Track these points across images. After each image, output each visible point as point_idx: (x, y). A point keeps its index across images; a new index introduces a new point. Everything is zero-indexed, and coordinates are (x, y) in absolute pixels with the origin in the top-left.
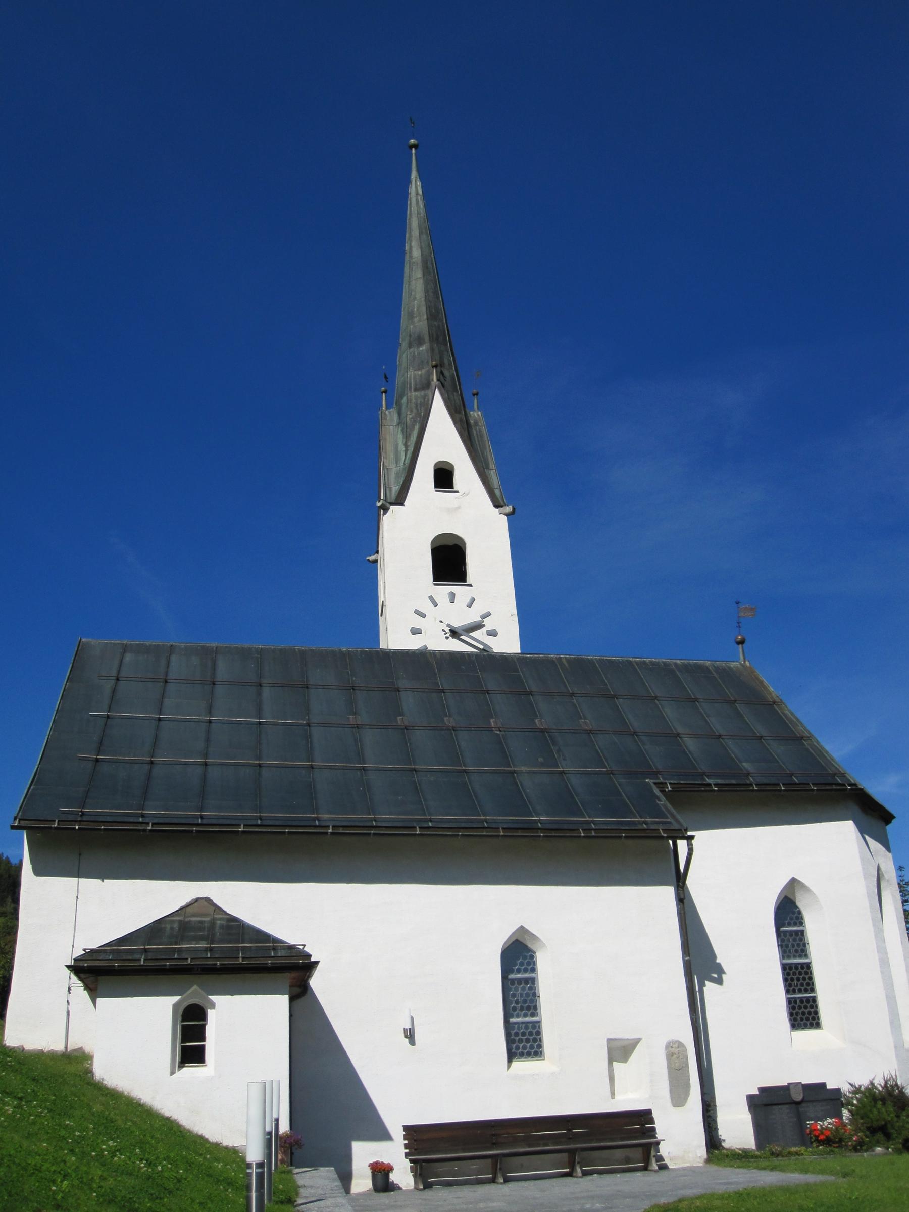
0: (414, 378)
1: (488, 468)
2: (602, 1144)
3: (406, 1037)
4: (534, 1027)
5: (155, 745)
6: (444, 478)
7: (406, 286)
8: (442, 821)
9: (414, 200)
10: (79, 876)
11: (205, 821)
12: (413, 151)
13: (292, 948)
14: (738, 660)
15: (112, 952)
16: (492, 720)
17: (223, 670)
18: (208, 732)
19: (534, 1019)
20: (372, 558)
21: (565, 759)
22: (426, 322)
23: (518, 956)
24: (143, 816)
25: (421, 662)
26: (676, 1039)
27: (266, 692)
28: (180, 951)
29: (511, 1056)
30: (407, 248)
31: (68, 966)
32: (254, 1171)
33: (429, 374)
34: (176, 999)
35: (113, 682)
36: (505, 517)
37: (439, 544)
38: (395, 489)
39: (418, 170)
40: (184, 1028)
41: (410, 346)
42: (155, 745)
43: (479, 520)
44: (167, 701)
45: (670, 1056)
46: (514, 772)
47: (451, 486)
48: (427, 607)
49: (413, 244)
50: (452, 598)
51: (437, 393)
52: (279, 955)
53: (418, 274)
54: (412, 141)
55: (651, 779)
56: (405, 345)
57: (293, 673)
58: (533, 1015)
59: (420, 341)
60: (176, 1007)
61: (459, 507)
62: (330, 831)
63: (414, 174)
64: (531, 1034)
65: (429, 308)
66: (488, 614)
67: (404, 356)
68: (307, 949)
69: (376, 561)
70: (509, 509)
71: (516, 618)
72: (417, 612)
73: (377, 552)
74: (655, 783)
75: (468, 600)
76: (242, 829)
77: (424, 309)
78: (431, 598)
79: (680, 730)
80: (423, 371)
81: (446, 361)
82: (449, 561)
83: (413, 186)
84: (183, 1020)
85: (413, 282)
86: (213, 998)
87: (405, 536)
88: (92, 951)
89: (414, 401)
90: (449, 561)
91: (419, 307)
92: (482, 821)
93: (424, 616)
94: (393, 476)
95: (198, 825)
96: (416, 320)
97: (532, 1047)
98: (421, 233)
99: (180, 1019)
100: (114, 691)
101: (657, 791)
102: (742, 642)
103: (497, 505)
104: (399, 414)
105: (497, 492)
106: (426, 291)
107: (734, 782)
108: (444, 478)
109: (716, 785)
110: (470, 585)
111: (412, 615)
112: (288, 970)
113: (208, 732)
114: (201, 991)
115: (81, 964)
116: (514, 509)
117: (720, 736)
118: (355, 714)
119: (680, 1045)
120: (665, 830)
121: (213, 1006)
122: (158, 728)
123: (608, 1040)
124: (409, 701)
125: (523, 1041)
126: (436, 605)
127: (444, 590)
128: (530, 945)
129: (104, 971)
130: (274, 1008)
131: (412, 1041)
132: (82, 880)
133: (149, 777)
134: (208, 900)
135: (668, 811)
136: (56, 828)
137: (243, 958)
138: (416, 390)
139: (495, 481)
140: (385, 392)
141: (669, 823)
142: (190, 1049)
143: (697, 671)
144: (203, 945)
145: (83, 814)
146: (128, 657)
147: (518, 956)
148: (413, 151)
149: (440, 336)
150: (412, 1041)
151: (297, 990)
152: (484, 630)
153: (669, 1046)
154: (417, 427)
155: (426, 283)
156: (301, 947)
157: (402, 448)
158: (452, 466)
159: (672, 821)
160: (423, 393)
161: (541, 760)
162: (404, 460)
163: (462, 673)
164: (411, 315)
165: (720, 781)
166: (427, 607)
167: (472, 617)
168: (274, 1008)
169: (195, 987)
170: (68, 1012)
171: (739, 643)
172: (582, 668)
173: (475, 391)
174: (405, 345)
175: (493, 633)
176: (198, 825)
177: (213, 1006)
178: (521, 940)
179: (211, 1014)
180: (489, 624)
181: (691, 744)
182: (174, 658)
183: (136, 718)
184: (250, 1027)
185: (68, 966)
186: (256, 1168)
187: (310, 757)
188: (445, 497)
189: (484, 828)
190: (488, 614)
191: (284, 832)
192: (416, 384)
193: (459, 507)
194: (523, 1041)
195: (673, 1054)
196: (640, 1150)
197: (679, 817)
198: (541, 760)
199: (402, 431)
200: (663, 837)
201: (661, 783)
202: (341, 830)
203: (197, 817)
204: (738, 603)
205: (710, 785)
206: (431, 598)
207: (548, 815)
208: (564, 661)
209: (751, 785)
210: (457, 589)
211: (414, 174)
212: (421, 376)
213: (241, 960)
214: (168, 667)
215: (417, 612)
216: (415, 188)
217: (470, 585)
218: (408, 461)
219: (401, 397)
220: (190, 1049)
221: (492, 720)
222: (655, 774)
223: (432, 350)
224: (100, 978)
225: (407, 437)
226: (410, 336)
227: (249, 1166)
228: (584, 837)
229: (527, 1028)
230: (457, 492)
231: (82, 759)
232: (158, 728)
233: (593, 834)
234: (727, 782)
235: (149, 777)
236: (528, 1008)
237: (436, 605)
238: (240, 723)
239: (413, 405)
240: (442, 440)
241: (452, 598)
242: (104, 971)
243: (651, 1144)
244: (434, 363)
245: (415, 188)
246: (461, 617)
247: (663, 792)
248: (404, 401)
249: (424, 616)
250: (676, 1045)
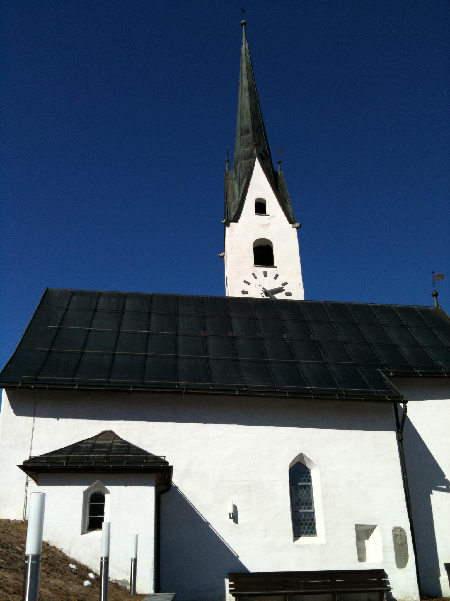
0: (244, 152)
1: (286, 202)
2: (353, 589)
3: (230, 518)
4: (310, 516)
5: (85, 344)
6: (261, 207)
7: (239, 102)
8: (252, 387)
9: (244, 54)
10: (34, 416)
11: (110, 385)
12: (244, 26)
13: (157, 458)
14: (432, 304)
15: (48, 458)
16: (284, 335)
17: (129, 305)
18: (117, 338)
19: (310, 511)
20: (221, 255)
21: (328, 357)
22: (250, 121)
23: (299, 474)
24: (73, 381)
25: (244, 304)
26: (399, 526)
27: (153, 318)
28: (88, 458)
29: (297, 535)
30: (240, 81)
31: (19, 466)
32: (30, 562)
33: (253, 150)
34: (86, 487)
35: (63, 311)
36: (295, 230)
37: (257, 245)
38: (233, 214)
39: (246, 38)
40: (91, 506)
41: (242, 134)
42: (85, 344)
43: (282, 233)
44: (95, 322)
45: (395, 536)
46: (298, 363)
47: (265, 213)
48: (251, 279)
49: (243, 78)
50: (265, 274)
51: (257, 161)
52: (149, 462)
53: (246, 94)
54: (243, 21)
55: (380, 369)
56: (239, 134)
57: (169, 306)
58: (309, 508)
59: (247, 132)
60: (86, 493)
61: (269, 224)
62: (185, 391)
63: (244, 39)
64: (308, 520)
65: (252, 113)
66: (286, 284)
67: (238, 141)
68: (167, 459)
69: (223, 256)
70: (297, 225)
71: (302, 286)
72: (245, 282)
73: (224, 251)
74: (383, 371)
75: (274, 275)
76: (132, 389)
77: (249, 114)
78: (253, 274)
79: (398, 342)
80: (249, 149)
81: (262, 143)
82: (263, 254)
83: (243, 46)
84: (91, 502)
85: (243, 100)
86: (108, 487)
87: (239, 239)
88: (36, 458)
89: (243, 165)
90: (263, 254)
91: (246, 113)
92: (276, 388)
93: (249, 284)
94: (232, 206)
95: (105, 386)
96: (245, 120)
97: (309, 528)
98: (248, 72)
99: (88, 500)
100: (64, 315)
101: (384, 376)
102: (436, 295)
103: (291, 222)
104: (236, 173)
105: (291, 216)
106: (251, 104)
107: (432, 372)
108: (261, 207)
109: (420, 373)
110: (276, 267)
111: (241, 279)
112: (155, 471)
113: (117, 338)
114: (100, 483)
115: (27, 465)
116: (301, 224)
117: (423, 346)
118: (204, 329)
119: (402, 530)
120: (389, 397)
121: (108, 492)
122: (88, 335)
123: (357, 526)
124: (236, 324)
125: (303, 523)
126: (256, 278)
127: (260, 270)
128: (308, 466)
129: (43, 469)
130: (144, 496)
131: (236, 521)
132: (37, 419)
133: (80, 361)
134: (111, 432)
135: (390, 385)
136: (19, 387)
137: (126, 463)
138: (245, 159)
139: (290, 210)
140: (228, 161)
141: (391, 393)
142: (94, 518)
143: (408, 311)
144: (104, 455)
145: (37, 379)
146: (75, 298)
147: (299, 474)
148: (244, 26)
149: (259, 128)
150: (236, 521)
151: (163, 487)
152: (284, 292)
153: (394, 530)
154: (245, 180)
155: (250, 99)
156: (163, 458)
157: (237, 191)
158: (265, 201)
159: (393, 392)
160: (249, 161)
161: (313, 357)
162: (238, 197)
163: (269, 308)
164: (242, 118)
165: (423, 371)
166: (251, 279)
167: (277, 284)
168: (144, 496)
169: (97, 481)
170: (26, 498)
171: (434, 296)
172: (338, 308)
173: (279, 161)
174: (239, 134)
175: (289, 294)
176: (105, 386)
177: (108, 492)
178: (301, 462)
179: (107, 497)
180: (287, 289)
181: (405, 351)
182: (101, 299)
183: (76, 330)
184: (131, 506)
185: (19, 466)
186: (32, 560)
187: (176, 352)
188: (261, 218)
189: (277, 392)
190: (286, 284)
191: (156, 392)
192: (245, 157)
193: (269, 224)
194: (303, 523)
195: (397, 536)
196: (377, 594)
197: (397, 390)
198: (313, 357)
199: (237, 182)
200: (387, 401)
201: (387, 371)
202: (191, 391)
203: (105, 382)
204: (433, 273)
205: (417, 373)
206: (253, 274)
207: (316, 386)
208: (328, 304)
209: (443, 373)
210: (268, 270)
211: (244, 39)
212: (248, 151)
213: (125, 464)
214: (97, 304)
215: (245, 282)
216: (244, 46)
217: (276, 267)
218: (240, 198)
219: (237, 164)
220: (94, 518)
221: (284, 335)
222: (382, 367)
223: (254, 136)
224: (40, 474)
225: (240, 186)
226: (242, 129)
227: (27, 558)
228: (338, 399)
229: (305, 516)
230: (268, 215)
231: (41, 351)
232: (88, 335)
233: (344, 397)
234: (428, 371)
235: (80, 361)
236: (306, 504)
237: (256, 278)
238: (136, 333)
239: (243, 168)
240: (260, 185)
241: (265, 274)
242: (43, 469)
243: (384, 590)
244: (255, 143)
245: (244, 46)
246: (271, 284)
247: (388, 376)
248: (238, 165)
249: (249, 284)
250: (399, 530)
